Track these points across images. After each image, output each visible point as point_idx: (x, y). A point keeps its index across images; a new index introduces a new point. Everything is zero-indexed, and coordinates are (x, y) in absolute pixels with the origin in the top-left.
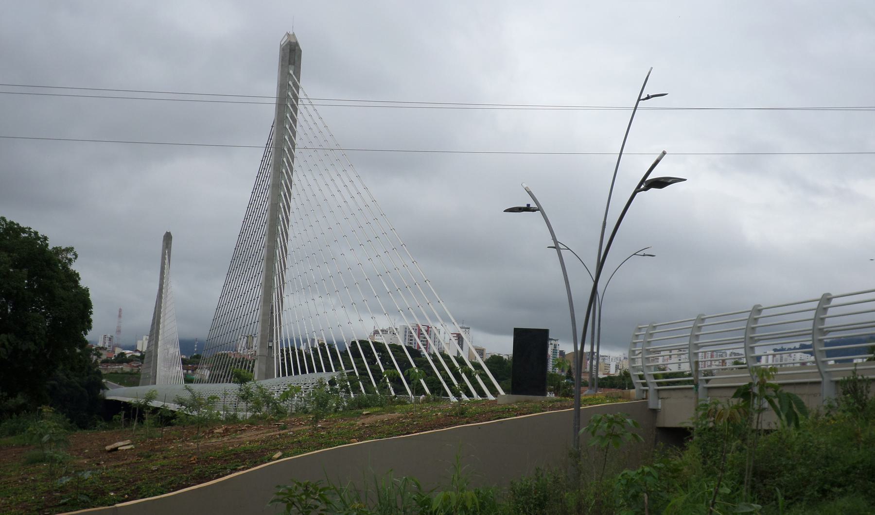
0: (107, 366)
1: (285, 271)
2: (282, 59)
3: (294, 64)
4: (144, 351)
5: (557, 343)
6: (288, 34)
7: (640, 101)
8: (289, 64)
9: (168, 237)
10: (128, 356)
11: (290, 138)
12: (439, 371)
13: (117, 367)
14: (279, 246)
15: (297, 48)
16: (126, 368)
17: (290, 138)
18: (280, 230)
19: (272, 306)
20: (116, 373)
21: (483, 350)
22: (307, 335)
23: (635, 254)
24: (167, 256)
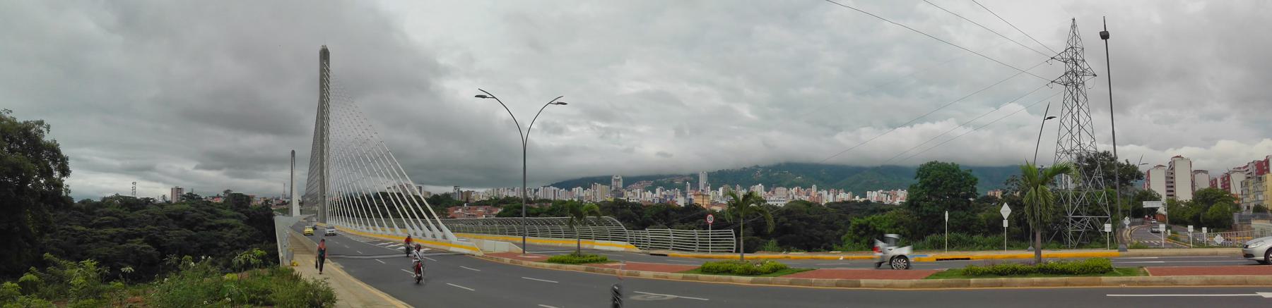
2: (321, 56)
11: (327, 79)
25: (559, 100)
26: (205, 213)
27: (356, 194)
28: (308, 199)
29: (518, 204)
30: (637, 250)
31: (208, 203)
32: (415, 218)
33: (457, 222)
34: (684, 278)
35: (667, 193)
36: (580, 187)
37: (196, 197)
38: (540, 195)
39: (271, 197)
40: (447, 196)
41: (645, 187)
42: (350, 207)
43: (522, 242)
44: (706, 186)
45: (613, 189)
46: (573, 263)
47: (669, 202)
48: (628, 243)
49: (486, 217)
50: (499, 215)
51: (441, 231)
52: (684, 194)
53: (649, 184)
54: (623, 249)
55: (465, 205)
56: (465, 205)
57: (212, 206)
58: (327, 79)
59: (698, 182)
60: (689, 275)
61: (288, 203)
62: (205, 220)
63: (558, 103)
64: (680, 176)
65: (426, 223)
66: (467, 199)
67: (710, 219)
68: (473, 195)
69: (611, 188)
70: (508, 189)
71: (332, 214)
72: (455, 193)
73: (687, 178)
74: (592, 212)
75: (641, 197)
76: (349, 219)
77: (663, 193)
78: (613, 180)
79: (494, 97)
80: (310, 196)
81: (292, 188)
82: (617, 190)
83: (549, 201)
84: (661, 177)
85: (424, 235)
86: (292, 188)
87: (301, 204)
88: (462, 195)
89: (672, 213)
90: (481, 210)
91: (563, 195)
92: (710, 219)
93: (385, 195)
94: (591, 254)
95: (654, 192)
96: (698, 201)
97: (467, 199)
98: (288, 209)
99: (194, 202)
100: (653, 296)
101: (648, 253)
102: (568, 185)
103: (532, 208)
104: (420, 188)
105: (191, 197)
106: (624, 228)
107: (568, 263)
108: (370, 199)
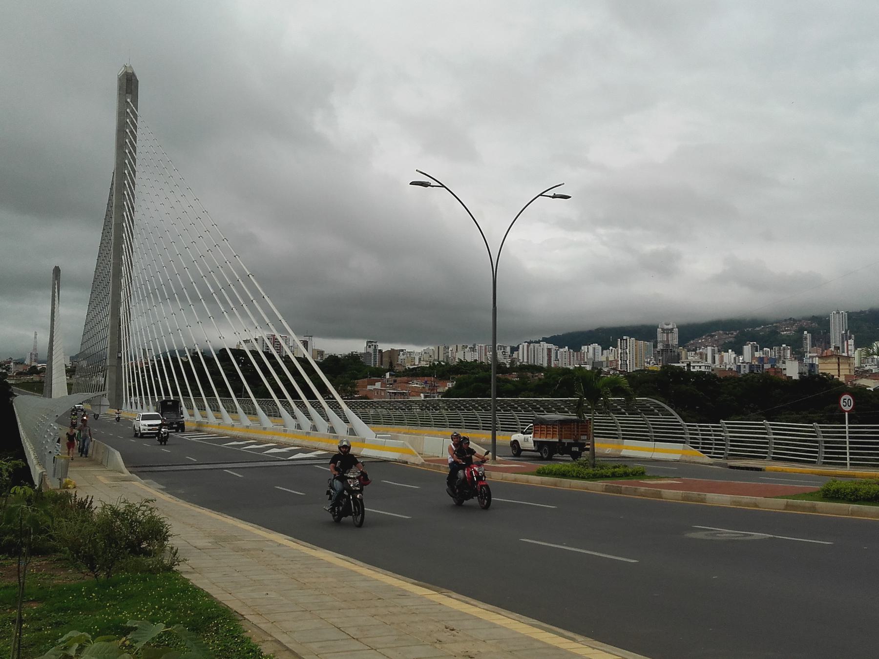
0: (21, 377)
1: (131, 284)
2: (120, 88)
3: (131, 93)
8: (127, 93)
10: (39, 368)
11: (131, 132)
13: (28, 377)
14: (124, 263)
16: (35, 378)
17: (131, 142)
18: (125, 226)
19: (120, 319)
20: (28, 382)
21: (323, 352)
22: (146, 344)
23: (541, 195)
24: (56, 290)
25: (557, 191)
27: (182, 353)
28: (84, 364)
29: (482, 374)
30: (705, 459)
32: (315, 398)
33: (372, 405)
34: (788, 507)
35: (766, 353)
38: (522, 357)
40: (354, 358)
41: (722, 342)
43: (490, 441)
44: (845, 338)
45: (660, 347)
46: (583, 478)
47: (768, 371)
48: (688, 446)
49: (426, 397)
50: (447, 394)
51: (310, 419)
52: (799, 355)
53: (730, 338)
54: (677, 457)
55: (388, 375)
56: (388, 375)
58: (131, 132)
59: (828, 331)
60: (798, 502)
64: (792, 321)
65: (301, 405)
66: (391, 364)
67: (846, 403)
68: (401, 357)
69: (655, 346)
71: (132, 392)
72: (367, 354)
74: (617, 390)
75: (714, 362)
76: (199, 401)
77: (757, 354)
79: (443, 186)
80: (87, 358)
82: (667, 348)
83: (540, 369)
84: (755, 323)
85: (314, 428)
87: (70, 372)
90: (416, 384)
91: (564, 358)
92: (846, 403)
93: (239, 353)
94: (615, 464)
95: (739, 352)
96: (828, 368)
97: (391, 364)
98: (41, 383)
100: (726, 533)
101: (725, 465)
103: (507, 381)
104: (305, 344)
106: (679, 419)
107: (573, 477)
108: (209, 360)
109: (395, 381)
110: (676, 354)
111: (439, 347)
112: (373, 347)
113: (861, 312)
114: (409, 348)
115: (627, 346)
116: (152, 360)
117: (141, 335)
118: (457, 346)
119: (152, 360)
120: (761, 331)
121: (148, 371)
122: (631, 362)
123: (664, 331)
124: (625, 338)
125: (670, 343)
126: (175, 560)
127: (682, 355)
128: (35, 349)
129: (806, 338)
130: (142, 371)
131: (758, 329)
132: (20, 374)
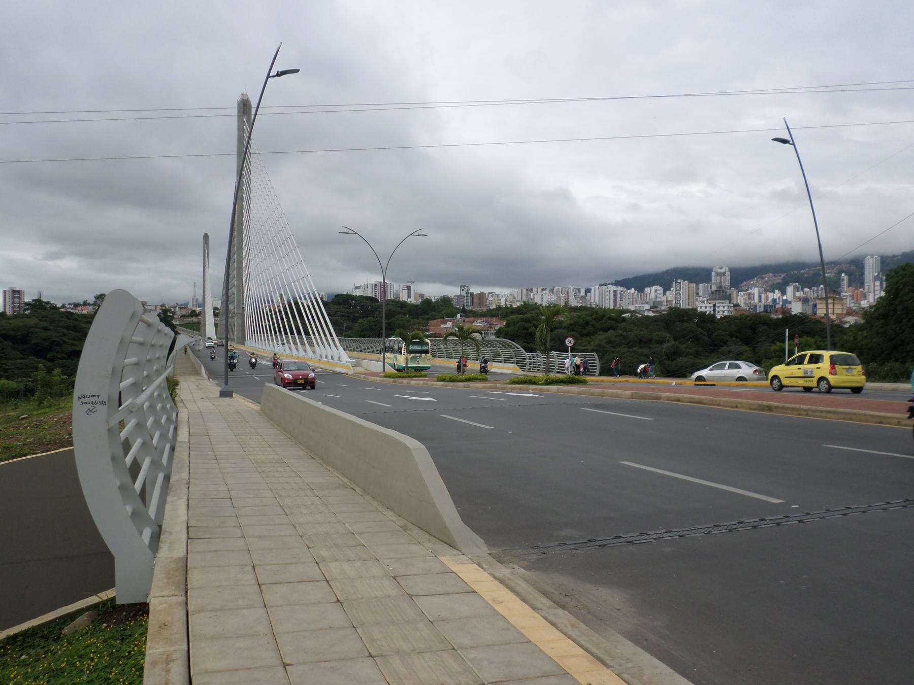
4: (544, 304)
5: (468, 288)
6: (242, 94)
7: (269, 78)
9: (206, 237)
10: (197, 312)
12: (275, 314)
15: (248, 103)
20: (189, 323)
21: (424, 295)
25: (420, 232)
26: (65, 331)
31: (69, 315)
35: (805, 293)
36: (658, 287)
37: (48, 306)
39: (173, 304)
41: (770, 283)
42: (294, 317)
48: (515, 365)
53: (778, 280)
55: (459, 316)
56: (459, 316)
57: (76, 320)
59: (863, 274)
61: (199, 314)
62: (65, 342)
63: (419, 235)
68: (490, 298)
70: (544, 289)
73: (844, 267)
77: (798, 294)
78: (713, 274)
79: (356, 233)
81: (204, 291)
86: (204, 291)
88: (473, 299)
89: (762, 328)
95: (784, 292)
98: (199, 323)
99: (44, 313)
102: (639, 282)
105: (38, 305)
109: (464, 321)
110: (728, 294)
111: (522, 290)
112: (465, 291)
113: (894, 256)
114: (498, 290)
115: (680, 288)
116: (279, 307)
117: (268, 285)
118: (537, 289)
119: (279, 307)
120: (805, 273)
121: (280, 312)
122: (684, 301)
123: (718, 275)
124: (679, 281)
125: (723, 284)
126: (56, 305)
127: (733, 294)
128: (195, 296)
129: (843, 280)
130: (276, 314)
131: (802, 271)
132: (183, 316)
